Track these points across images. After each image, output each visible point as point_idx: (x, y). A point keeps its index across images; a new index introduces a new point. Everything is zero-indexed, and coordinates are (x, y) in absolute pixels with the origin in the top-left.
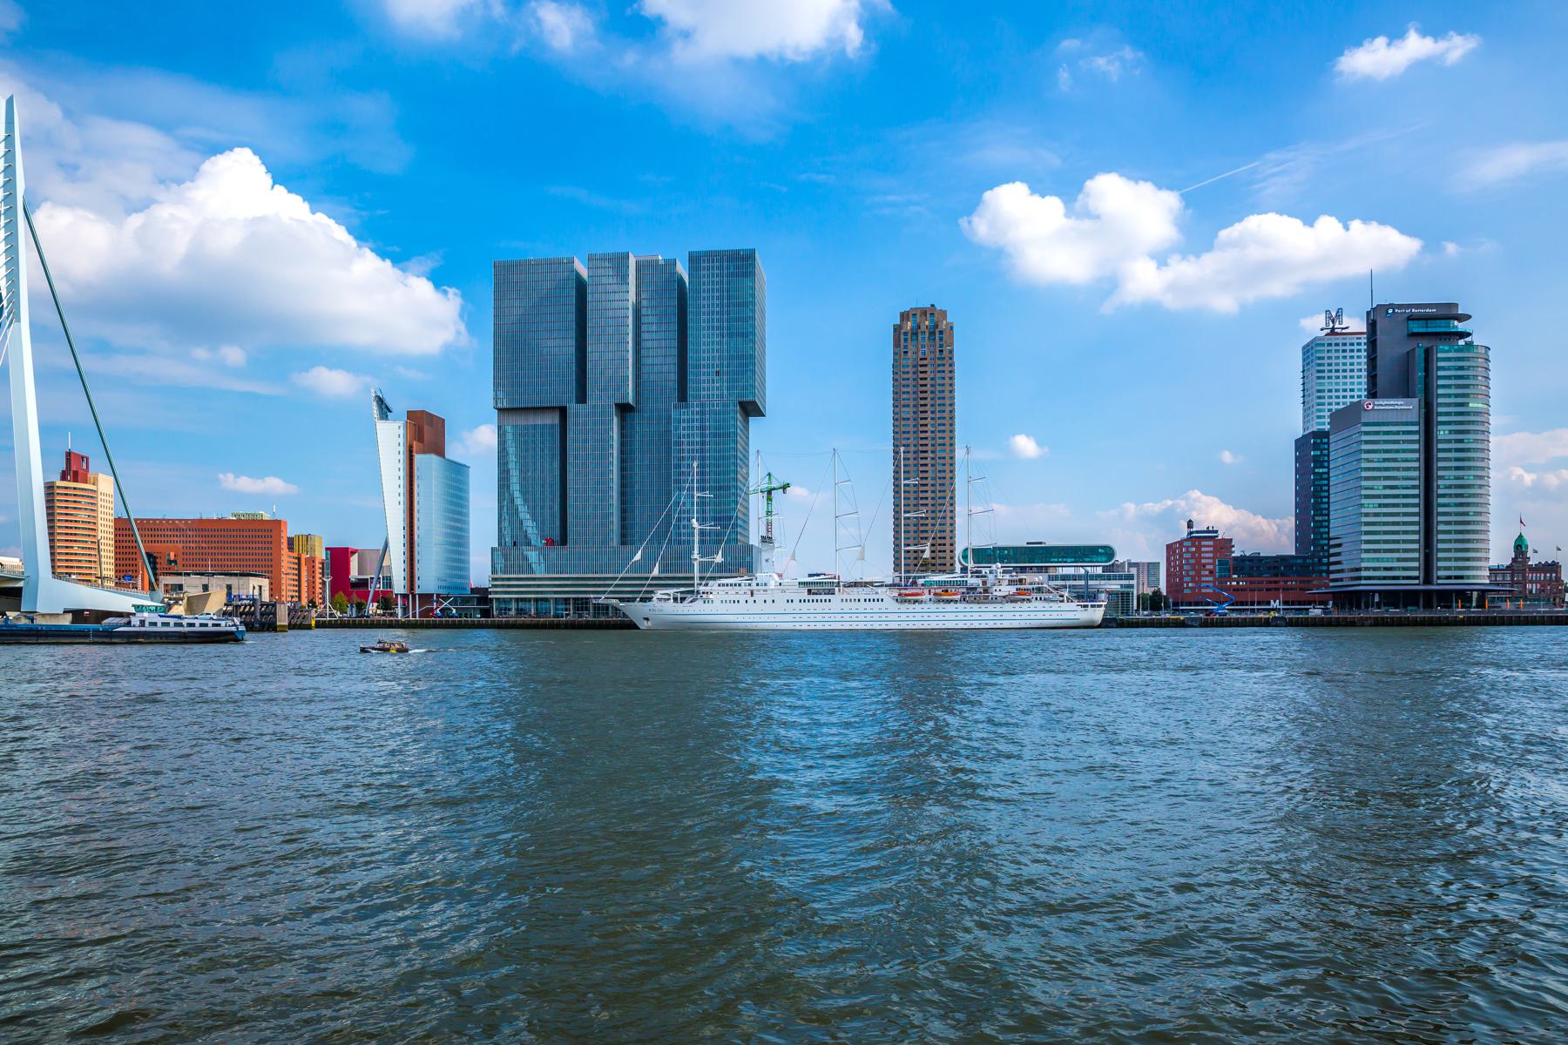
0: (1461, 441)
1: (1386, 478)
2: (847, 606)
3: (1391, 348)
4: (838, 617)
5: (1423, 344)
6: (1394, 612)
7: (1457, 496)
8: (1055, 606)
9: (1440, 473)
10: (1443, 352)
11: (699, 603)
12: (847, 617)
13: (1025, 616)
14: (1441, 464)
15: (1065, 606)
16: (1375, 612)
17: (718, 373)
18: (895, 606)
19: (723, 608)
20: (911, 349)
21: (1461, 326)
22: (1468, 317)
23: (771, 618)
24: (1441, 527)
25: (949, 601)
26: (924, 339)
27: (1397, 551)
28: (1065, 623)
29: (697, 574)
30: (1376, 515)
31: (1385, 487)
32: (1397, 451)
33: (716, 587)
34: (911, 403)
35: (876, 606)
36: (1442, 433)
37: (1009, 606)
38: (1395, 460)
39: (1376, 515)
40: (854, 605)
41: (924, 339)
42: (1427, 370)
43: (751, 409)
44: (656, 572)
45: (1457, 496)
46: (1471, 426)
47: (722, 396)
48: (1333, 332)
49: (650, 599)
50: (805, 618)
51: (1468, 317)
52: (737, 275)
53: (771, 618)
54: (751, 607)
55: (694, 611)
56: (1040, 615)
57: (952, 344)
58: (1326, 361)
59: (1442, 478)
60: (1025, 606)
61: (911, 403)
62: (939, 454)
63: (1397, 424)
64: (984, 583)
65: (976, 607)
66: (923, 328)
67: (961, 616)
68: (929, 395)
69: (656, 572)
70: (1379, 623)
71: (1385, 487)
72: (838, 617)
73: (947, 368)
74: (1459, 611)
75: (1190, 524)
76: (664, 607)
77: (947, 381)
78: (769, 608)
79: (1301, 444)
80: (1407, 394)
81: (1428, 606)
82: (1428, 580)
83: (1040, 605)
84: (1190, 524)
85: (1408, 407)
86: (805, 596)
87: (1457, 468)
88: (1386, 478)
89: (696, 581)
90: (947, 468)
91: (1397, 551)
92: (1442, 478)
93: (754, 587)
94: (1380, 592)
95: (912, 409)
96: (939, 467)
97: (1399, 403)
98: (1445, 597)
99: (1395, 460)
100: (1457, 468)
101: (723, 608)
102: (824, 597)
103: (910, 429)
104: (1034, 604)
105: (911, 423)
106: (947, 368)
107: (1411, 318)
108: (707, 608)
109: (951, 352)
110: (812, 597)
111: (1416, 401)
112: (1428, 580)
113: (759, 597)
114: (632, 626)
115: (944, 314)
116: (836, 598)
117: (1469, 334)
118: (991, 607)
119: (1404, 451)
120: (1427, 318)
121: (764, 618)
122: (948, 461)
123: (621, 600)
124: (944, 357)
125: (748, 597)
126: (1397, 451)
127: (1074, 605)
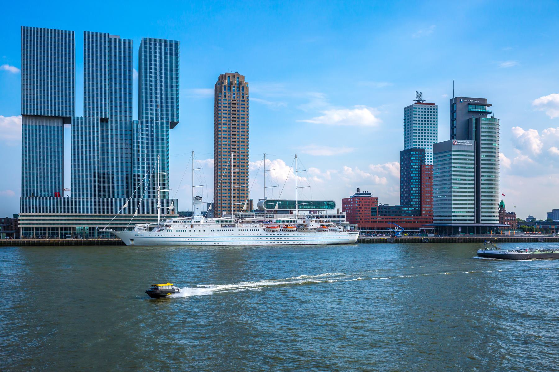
0: (490, 160)
1: (462, 176)
2: (241, 233)
3: (461, 118)
4: (237, 239)
5: (474, 117)
6: (467, 236)
7: (489, 184)
8: (338, 233)
9: (482, 174)
10: (483, 121)
11: (165, 231)
12: (241, 239)
13: (325, 238)
14: (483, 170)
15: (342, 233)
16: (460, 236)
17: (158, 106)
18: (264, 234)
19: (177, 234)
20: (228, 94)
21: (488, 109)
22: (491, 105)
23: (203, 239)
24: (483, 198)
25: (290, 231)
26: (234, 90)
27: (466, 208)
28: (343, 242)
29: (159, 215)
30: (458, 192)
31: (461, 180)
32: (466, 164)
33: (172, 223)
34: (228, 123)
35: (256, 233)
36: (483, 156)
37: (318, 234)
38: (465, 168)
39: (458, 192)
40: (245, 233)
41: (234, 90)
42: (476, 128)
43: (173, 125)
44: (136, 214)
45: (489, 184)
46: (493, 153)
47: (161, 118)
48: (419, 102)
49: (132, 229)
50: (220, 239)
51: (491, 105)
52: (170, 54)
53: (203, 239)
54: (193, 234)
55: (156, 235)
56: (332, 238)
57: (248, 94)
58: (417, 116)
59: (483, 176)
60: (325, 233)
61: (228, 123)
62: (241, 150)
63: (458, 151)
64: (304, 222)
65: (303, 234)
66: (234, 84)
67: (296, 238)
68: (236, 119)
69: (136, 214)
70: (466, 241)
71: (461, 180)
72: (237, 239)
73: (246, 106)
74: (492, 235)
75: (358, 190)
76: (141, 232)
77: (246, 113)
78: (202, 234)
79: (402, 153)
80: (468, 138)
81: (478, 233)
82: (478, 222)
83: (332, 233)
84: (358, 190)
85: (470, 144)
86: (220, 228)
87: (489, 172)
88: (462, 176)
89: (159, 219)
90: (245, 158)
91: (466, 208)
92: (483, 176)
93: (193, 223)
94: (461, 226)
95: (227, 126)
96: (241, 157)
97: (467, 142)
98: (486, 230)
99: (465, 168)
100: (489, 172)
101: (177, 234)
102: (230, 229)
103: (227, 136)
104: (328, 233)
105: (227, 133)
106: (246, 106)
107: (470, 104)
108: (169, 234)
109: (248, 98)
110: (223, 229)
111: (473, 141)
112: (478, 222)
113: (196, 228)
114: (121, 243)
115: (243, 77)
116: (236, 229)
117: (491, 113)
118: (310, 234)
119: (468, 164)
120: (476, 105)
121: (199, 239)
122: (245, 154)
123: (116, 229)
124: (244, 99)
125: (190, 228)
126: (466, 164)
127: (346, 233)
